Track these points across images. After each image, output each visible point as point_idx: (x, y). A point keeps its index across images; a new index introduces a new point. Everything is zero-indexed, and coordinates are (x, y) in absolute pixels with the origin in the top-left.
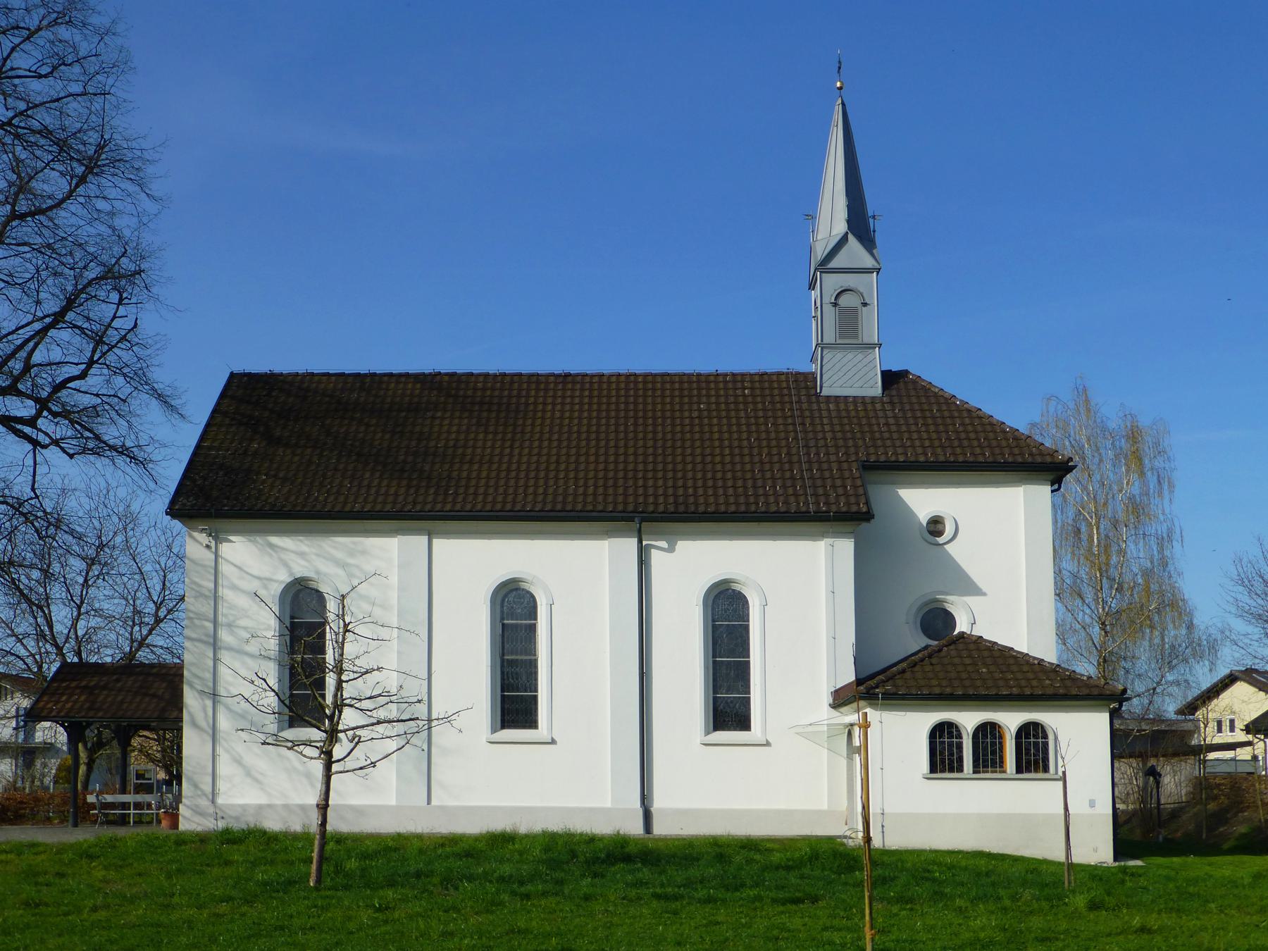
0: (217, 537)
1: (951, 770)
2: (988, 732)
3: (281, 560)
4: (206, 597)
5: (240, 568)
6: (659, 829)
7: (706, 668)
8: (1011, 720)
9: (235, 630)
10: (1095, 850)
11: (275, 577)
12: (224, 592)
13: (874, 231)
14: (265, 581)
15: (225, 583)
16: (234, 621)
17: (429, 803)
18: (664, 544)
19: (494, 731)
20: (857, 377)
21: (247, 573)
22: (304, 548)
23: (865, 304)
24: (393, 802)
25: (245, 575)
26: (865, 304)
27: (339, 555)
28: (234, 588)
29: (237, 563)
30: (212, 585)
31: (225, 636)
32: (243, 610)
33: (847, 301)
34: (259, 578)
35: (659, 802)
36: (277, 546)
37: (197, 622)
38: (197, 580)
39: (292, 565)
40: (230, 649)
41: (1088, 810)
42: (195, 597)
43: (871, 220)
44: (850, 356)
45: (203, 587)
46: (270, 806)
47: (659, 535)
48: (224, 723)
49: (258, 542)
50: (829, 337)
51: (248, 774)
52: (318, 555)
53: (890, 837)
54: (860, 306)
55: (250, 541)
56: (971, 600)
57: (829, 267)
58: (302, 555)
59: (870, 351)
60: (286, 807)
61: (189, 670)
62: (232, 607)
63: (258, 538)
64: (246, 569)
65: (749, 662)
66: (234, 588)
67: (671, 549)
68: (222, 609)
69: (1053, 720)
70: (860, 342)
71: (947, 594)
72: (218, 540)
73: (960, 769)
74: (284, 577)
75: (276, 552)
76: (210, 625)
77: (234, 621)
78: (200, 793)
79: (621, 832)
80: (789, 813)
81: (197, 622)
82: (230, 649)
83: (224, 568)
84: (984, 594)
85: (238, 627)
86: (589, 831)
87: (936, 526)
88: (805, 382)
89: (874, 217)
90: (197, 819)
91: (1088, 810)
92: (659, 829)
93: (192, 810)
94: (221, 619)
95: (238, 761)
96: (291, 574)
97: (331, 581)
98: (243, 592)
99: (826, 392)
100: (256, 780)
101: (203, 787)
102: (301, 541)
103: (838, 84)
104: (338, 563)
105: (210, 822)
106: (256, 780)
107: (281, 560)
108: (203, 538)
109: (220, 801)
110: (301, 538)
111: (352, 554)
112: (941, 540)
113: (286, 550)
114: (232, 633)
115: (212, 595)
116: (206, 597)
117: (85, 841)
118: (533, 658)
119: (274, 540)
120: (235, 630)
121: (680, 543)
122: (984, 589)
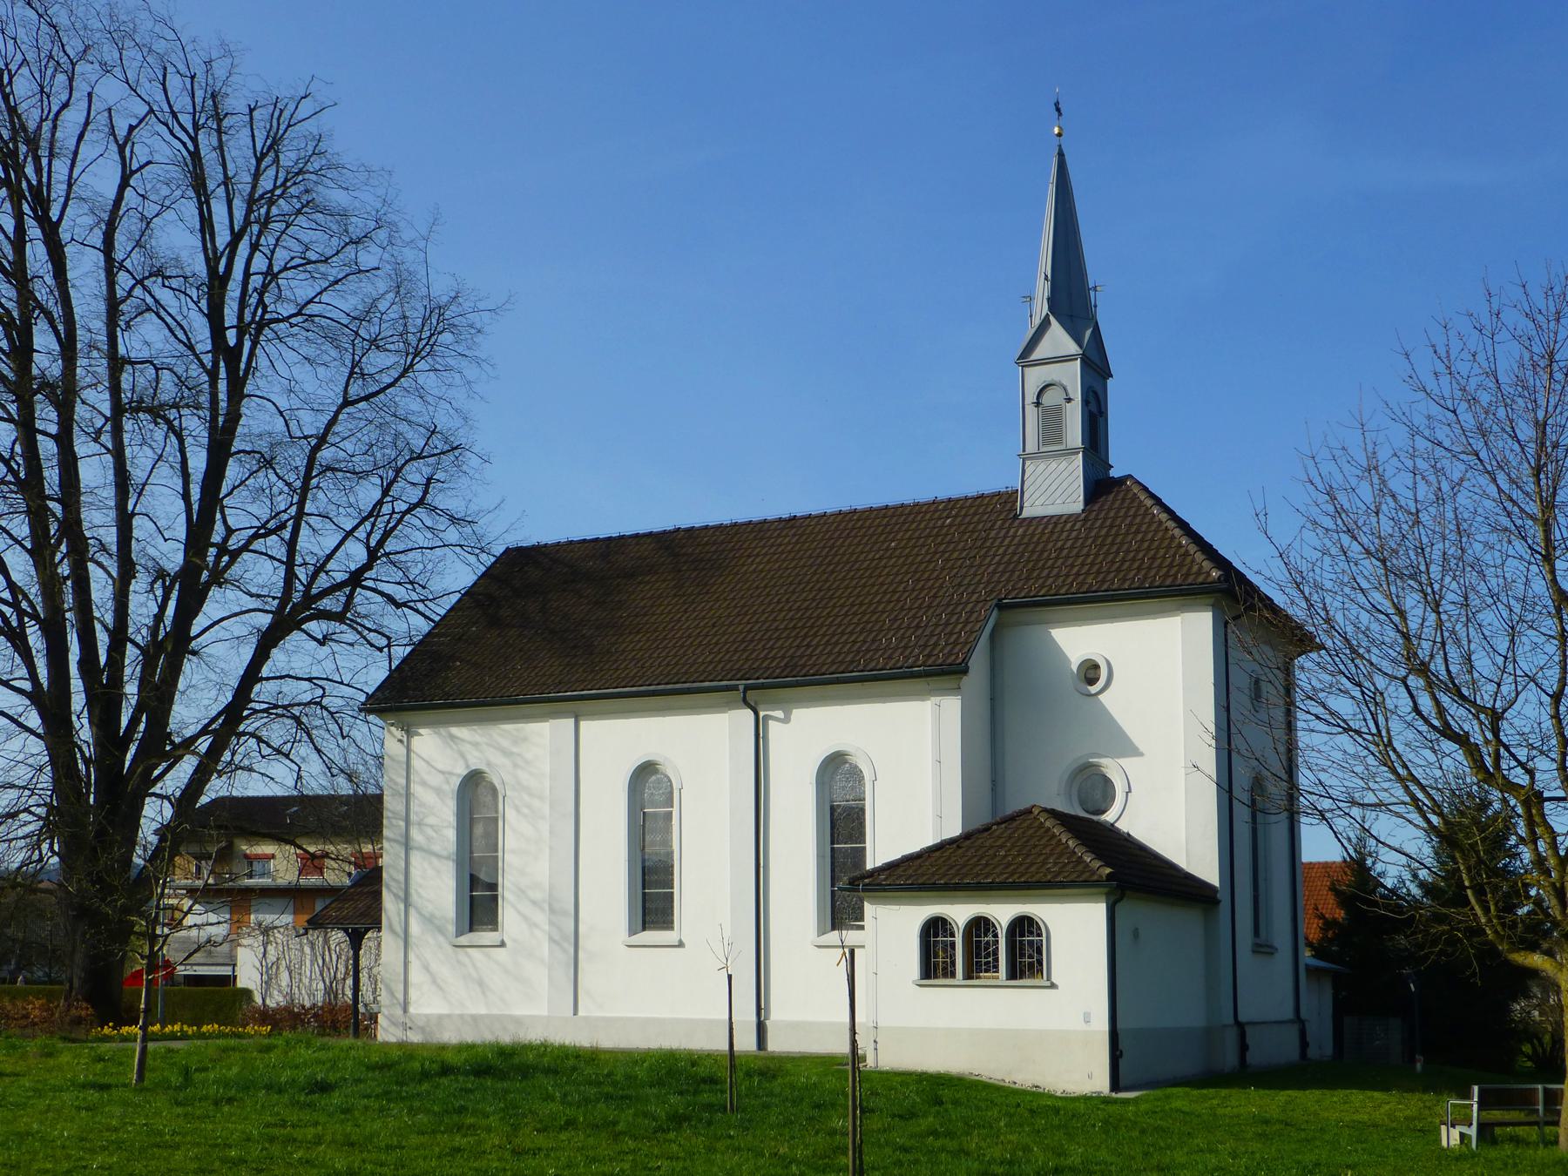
1: (945, 976)
2: (980, 925)
4: (401, 795)
5: (428, 762)
6: (775, 1045)
7: (820, 856)
8: (1002, 913)
10: (1090, 1077)
11: (455, 771)
12: (416, 788)
13: (1095, 306)
14: (446, 774)
15: (416, 779)
17: (575, 1013)
18: (779, 714)
19: (632, 932)
20: (1060, 491)
21: (433, 767)
22: (478, 738)
23: (1069, 400)
24: (545, 1013)
26: (1069, 400)
27: (505, 743)
28: (424, 783)
30: (403, 781)
31: (415, 834)
34: (442, 772)
35: (778, 1014)
36: (457, 738)
39: (469, 757)
40: (420, 849)
41: (1082, 1026)
42: (393, 795)
43: (1092, 293)
44: (1054, 465)
46: (449, 1016)
47: (776, 704)
48: (415, 927)
50: (1031, 446)
51: (434, 981)
53: (887, 1056)
55: (436, 733)
57: (1032, 358)
58: (476, 745)
59: (1073, 457)
60: (461, 1016)
61: (388, 872)
62: (422, 805)
63: (441, 729)
64: (433, 764)
65: (864, 848)
66: (424, 783)
67: (786, 720)
68: (414, 807)
69: (1045, 911)
70: (1063, 447)
72: (410, 734)
73: (953, 975)
74: (462, 771)
75: (456, 744)
76: (402, 824)
77: (422, 820)
82: (420, 849)
83: (415, 762)
84: (1141, 754)
85: (426, 825)
87: (1090, 671)
88: (1007, 502)
89: (1095, 289)
90: (392, 1029)
91: (1084, 1027)
92: (775, 1045)
94: (413, 817)
95: (426, 968)
96: (468, 766)
97: (500, 772)
99: (1027, 513)
100: (440, 988)
102: (475, 730)
103: (1056, 130)
106: (440, 988)
108: (398, 733)
109: (412, 1010)
110: (475, 727)
111: (515, 742)
112: (1093, 689)
113: (463, 740)
115: (403, 792)
116: (401, 795)
117: (466, 1061)
119: (455, 730)
121: (795, 711)
122: (1142, 748)
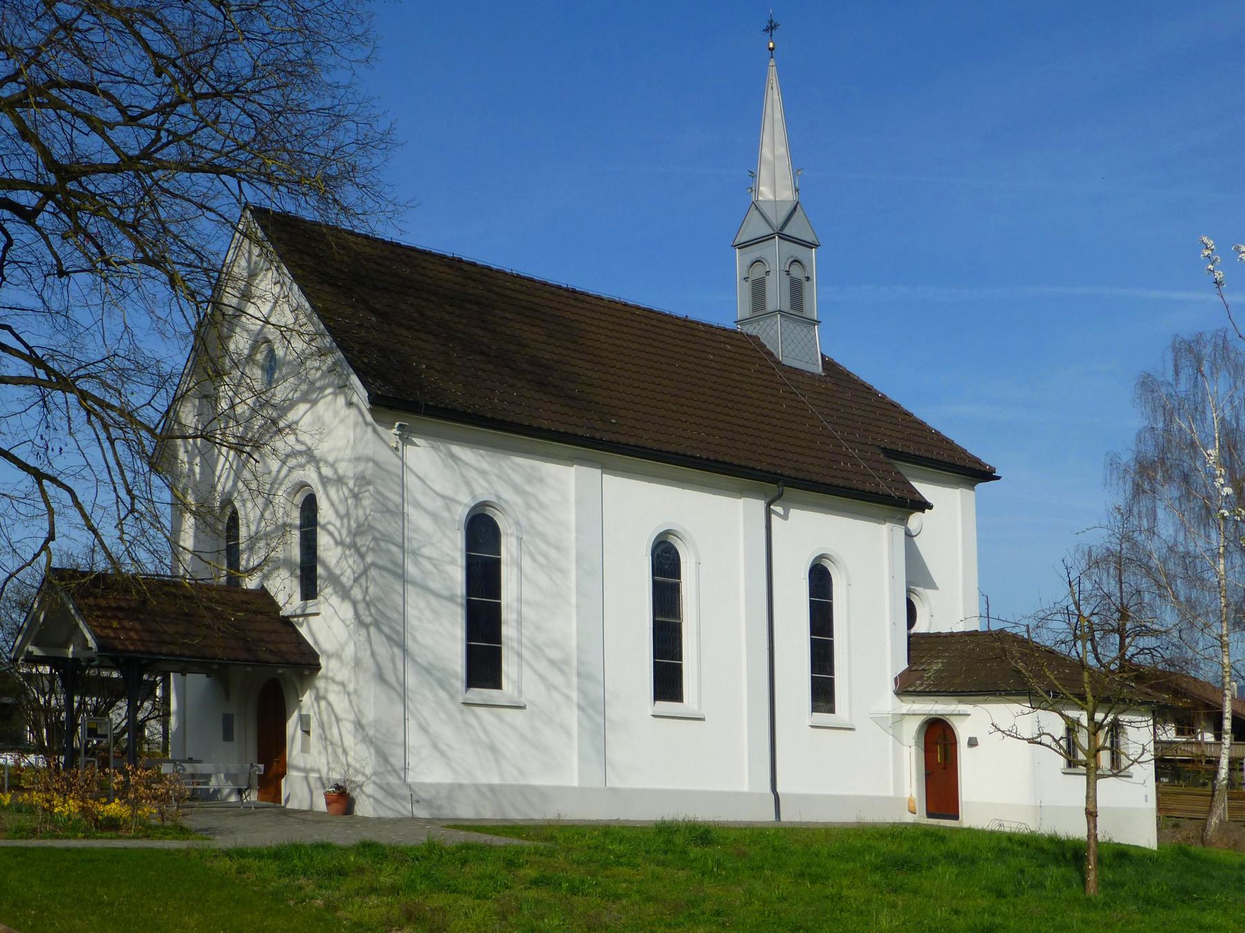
0: (405, 438)
3: (463, 476)
6: (785, 817)
9: (420, 559)
14: (448, 501)
16: (419, 549)
22: (485, 466)
24: (576, 784)
25: (429, 491)
27: (517, 478)
28: (417, 505)
29: (421, 474)
32: (428, 535)
33: (796, 271)
34: (442, 497)
37: (382, 544)
38: (382, 490)
39: (474, 485)
45: (389, 500)
49: (440, 451)
52: (498, 477)
54: (804, 280)
55: (433, 447)
56: (929, 592)
58: (483, 473)
71: (919, 586)
77: (419, 549)
78: (390, 768)
79: (1058, 833)
80: (843, 799)
81: (382, 544)
86: (871, 821)
93: (385, 790)
95: (424, 729)
98: (425, 510)
100: (442, 753)
101: (393, 760)
103: (771, 45)
104: (517, 489)
105: (404, 807)
106: (442, 753)
107: (463, 476)
110: (482, 452)
114: (417, 564)
118: (677, 621)
119: (457, 449)
120: (420, 559)
